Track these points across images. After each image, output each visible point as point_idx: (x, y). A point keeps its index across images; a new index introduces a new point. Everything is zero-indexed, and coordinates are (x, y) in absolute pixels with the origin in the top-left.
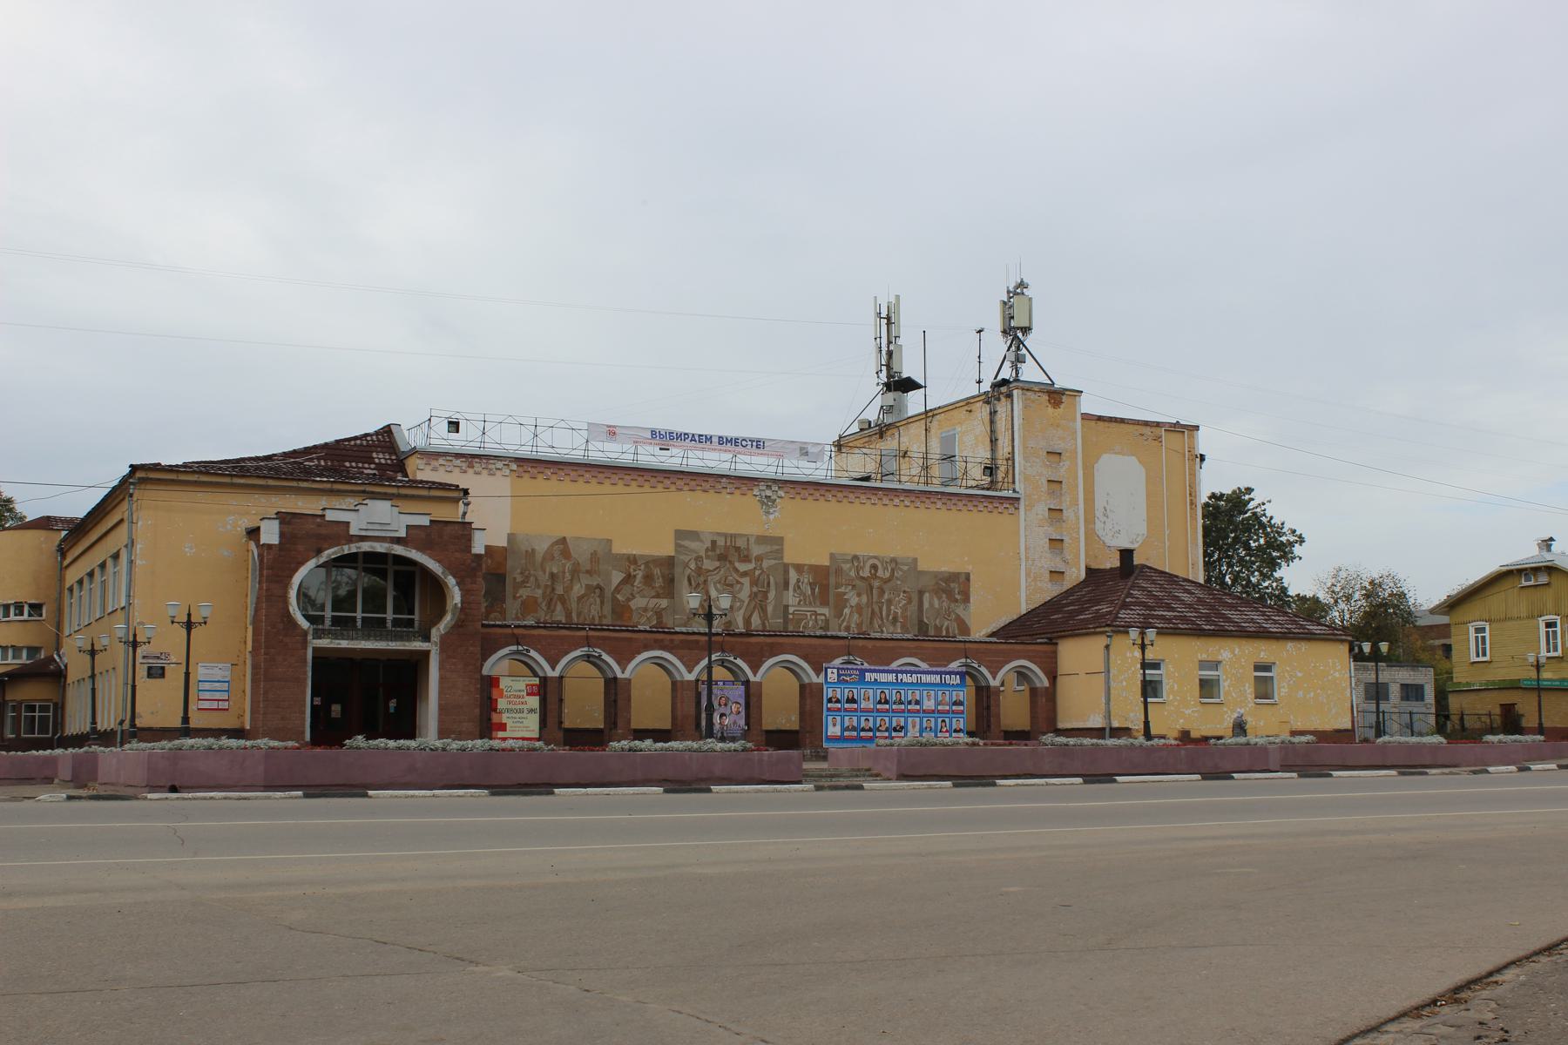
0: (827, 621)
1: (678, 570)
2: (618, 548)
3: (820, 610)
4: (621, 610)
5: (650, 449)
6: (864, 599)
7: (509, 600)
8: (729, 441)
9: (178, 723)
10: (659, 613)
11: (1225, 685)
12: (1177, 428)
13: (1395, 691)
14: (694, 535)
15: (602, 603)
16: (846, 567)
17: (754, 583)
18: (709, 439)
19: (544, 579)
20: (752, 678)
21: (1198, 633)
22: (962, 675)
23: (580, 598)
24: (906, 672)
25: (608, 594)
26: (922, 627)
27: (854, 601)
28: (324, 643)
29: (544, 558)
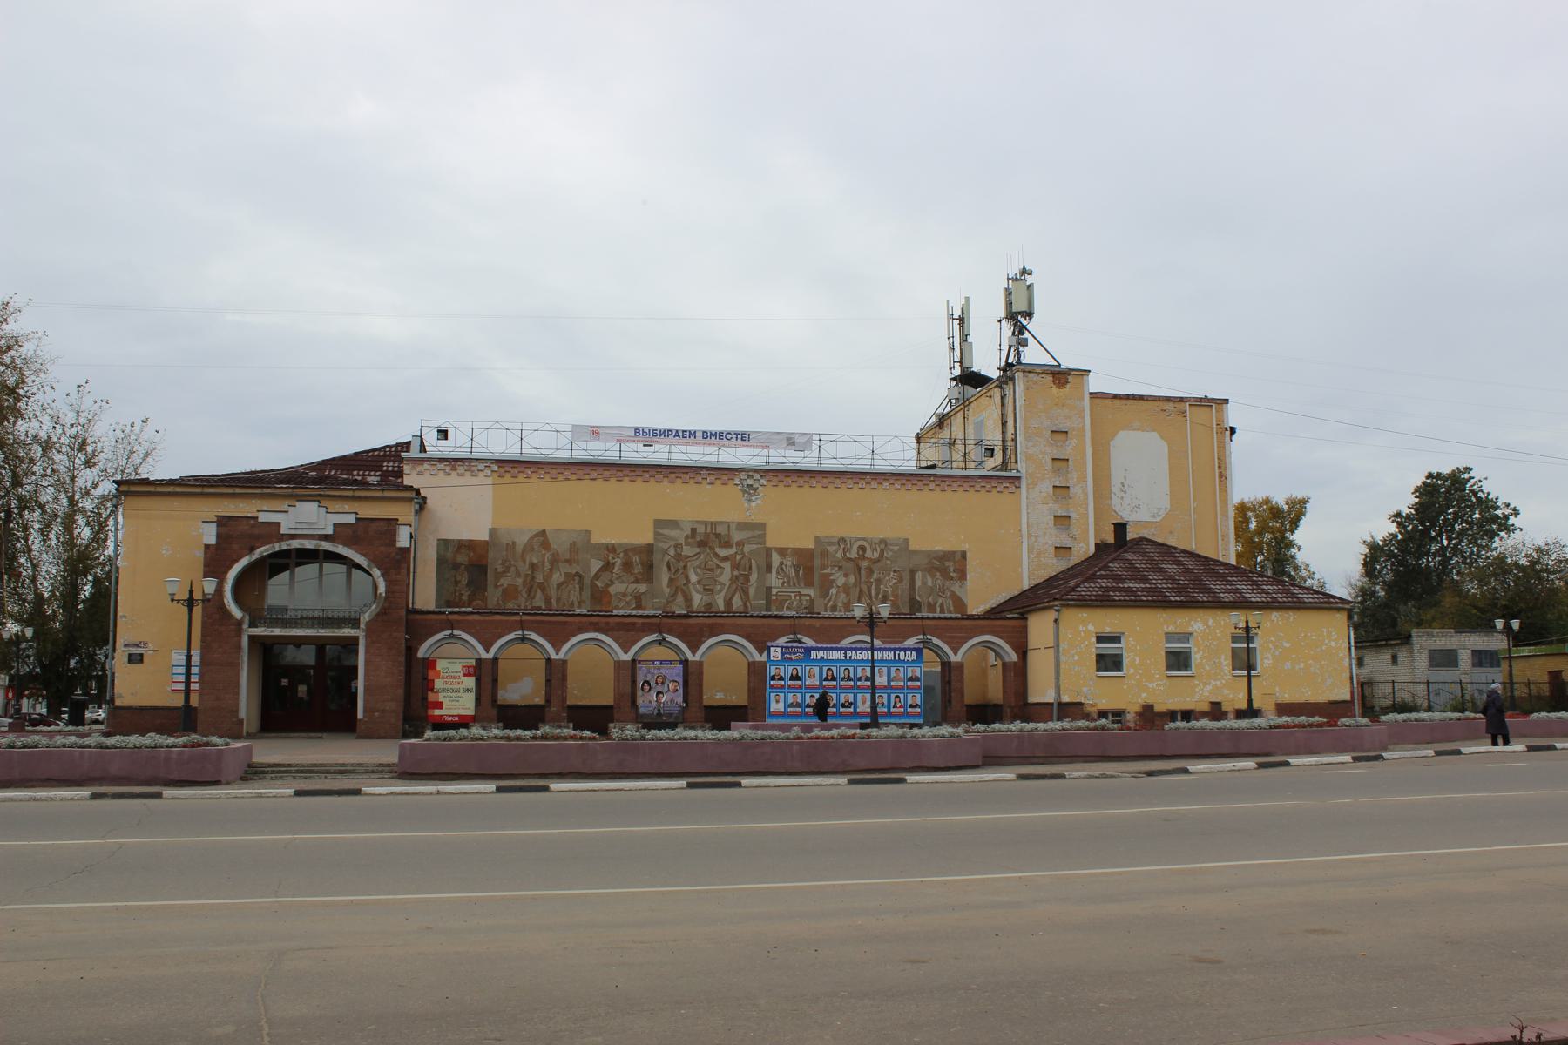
0: (812, 601)
1: (657, 557)
2: (597, 538)
3: (804, 591)
4: (599, 596)
5: (634, 446)
6: (852, 579)
7: (490, 589)
8: (714, 435)
9: (1244, 706)
10: (638, 598)
11: (1196, 658)
12: (1205, 403)
13: (1465, 658)
14: (674, 524)
15: (581, 589)
16: (831, 549)
17: (735, 566)
18: (693, 434)
19: (525, 568)
20: (690, 657)
21: (1163, 603)
22: (919, 652)
23: (559, 586)
24: (856, 649)
25: (587, 581)
26: (915, 606)
27: (841, 581)
28: (259, 631)
29: (524, 551)
